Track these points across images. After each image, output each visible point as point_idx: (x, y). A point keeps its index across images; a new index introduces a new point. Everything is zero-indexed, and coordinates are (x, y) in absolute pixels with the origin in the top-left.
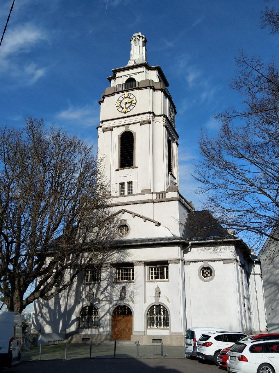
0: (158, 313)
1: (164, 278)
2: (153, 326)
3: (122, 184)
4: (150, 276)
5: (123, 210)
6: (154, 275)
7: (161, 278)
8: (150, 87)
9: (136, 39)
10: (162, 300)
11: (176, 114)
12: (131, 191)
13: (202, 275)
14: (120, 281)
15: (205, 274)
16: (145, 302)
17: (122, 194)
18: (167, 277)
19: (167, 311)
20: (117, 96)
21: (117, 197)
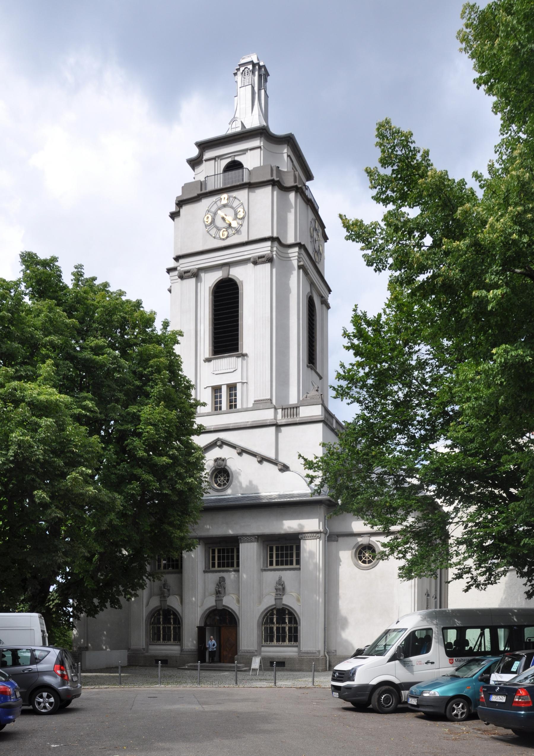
0: (281, 620)
1: (292, 564)
2: (272, 641)
3: (217, 390)
4: (269, 560)
5: (218, 440)
6: (274, 559)
7: (287, 564)
8: (273, 183)
9: (246, 70)
10: (288, 601)
11: (326, 242)
12: (233, 403)
13: (370, 564)
14: (216, 568)
15: (368, 558)
16: (260, 602)
17: (217, 408)
18: (298, 562)
19: (295, 618)
20: (206, 202)
21: (208, 415)
